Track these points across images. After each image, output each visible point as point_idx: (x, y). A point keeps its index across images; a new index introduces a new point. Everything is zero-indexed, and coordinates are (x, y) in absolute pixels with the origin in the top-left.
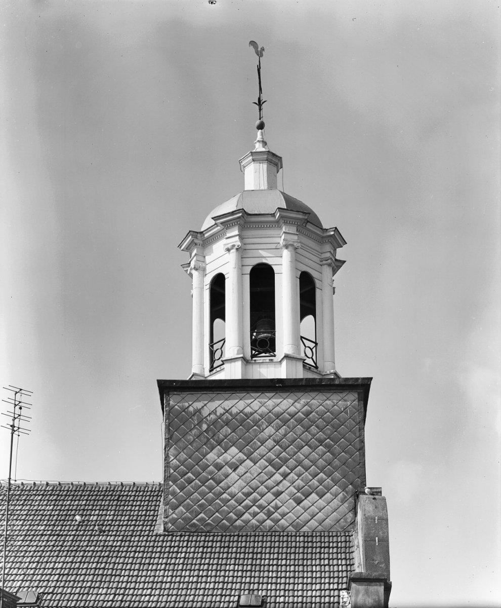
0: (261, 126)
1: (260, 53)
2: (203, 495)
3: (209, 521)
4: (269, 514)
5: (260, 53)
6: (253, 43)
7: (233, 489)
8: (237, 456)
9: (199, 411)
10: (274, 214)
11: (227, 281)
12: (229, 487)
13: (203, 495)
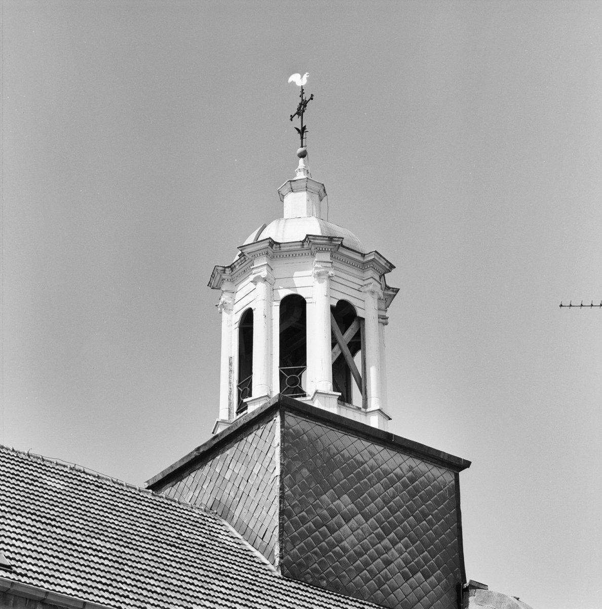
0: (303, 155)
2: (316, 539)
3: (322, 575)
4: (380, 584)
5: (312, 99)
7: (345, 543)
8: (350, 506)
10: (365, 255)
12: (342, 541)
13: (316, 539)
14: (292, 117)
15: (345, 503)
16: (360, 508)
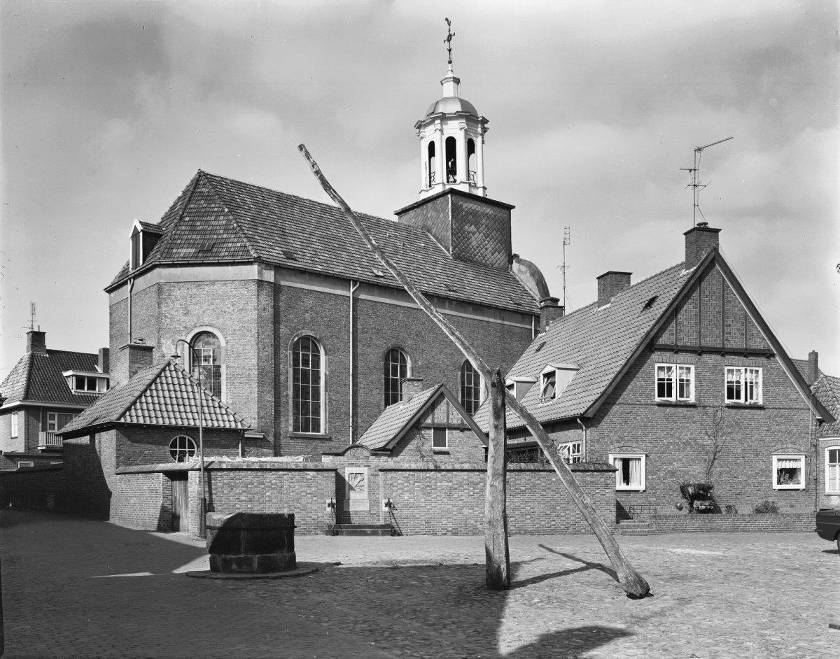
0: (450, 62)
1: (449, 24)
5: (449, 24)
6: (447, 20)
9: (462, 205)
11: (457, 143)
14: (444, 41)
15: (473, 228)
16: (478, 230)
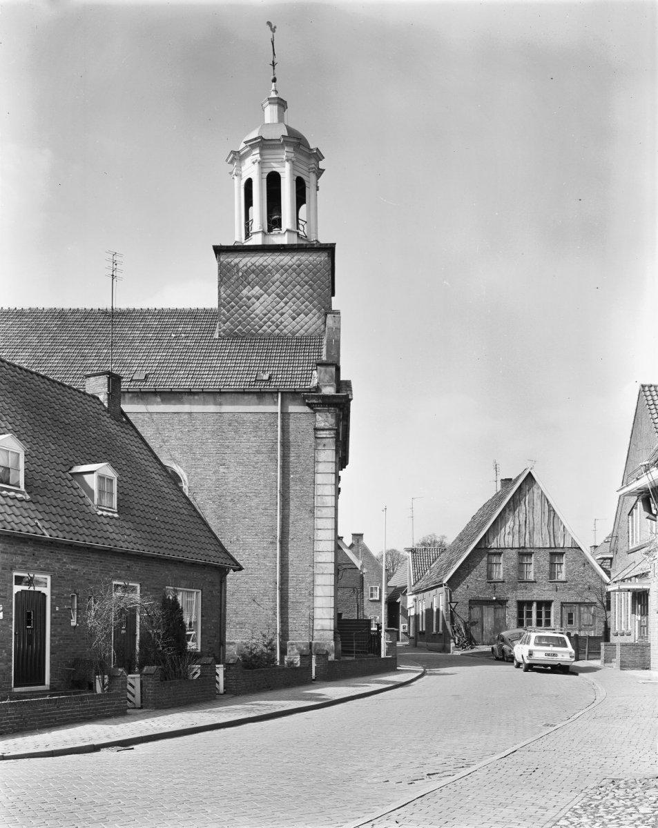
0: (274, 80)
1: (273, 30)
2: (240, 315)
4: (277, 326)
5: (273, 30)
6: (269, 23)
9: (237, 264)
13: (240, 315)
16: (265, 292)
